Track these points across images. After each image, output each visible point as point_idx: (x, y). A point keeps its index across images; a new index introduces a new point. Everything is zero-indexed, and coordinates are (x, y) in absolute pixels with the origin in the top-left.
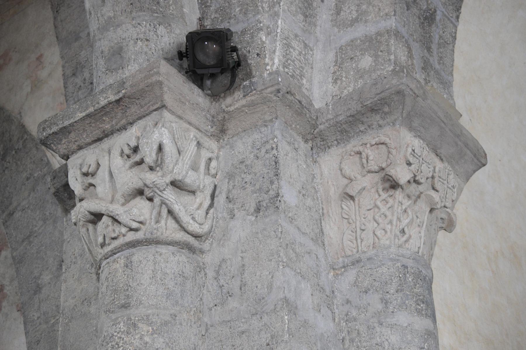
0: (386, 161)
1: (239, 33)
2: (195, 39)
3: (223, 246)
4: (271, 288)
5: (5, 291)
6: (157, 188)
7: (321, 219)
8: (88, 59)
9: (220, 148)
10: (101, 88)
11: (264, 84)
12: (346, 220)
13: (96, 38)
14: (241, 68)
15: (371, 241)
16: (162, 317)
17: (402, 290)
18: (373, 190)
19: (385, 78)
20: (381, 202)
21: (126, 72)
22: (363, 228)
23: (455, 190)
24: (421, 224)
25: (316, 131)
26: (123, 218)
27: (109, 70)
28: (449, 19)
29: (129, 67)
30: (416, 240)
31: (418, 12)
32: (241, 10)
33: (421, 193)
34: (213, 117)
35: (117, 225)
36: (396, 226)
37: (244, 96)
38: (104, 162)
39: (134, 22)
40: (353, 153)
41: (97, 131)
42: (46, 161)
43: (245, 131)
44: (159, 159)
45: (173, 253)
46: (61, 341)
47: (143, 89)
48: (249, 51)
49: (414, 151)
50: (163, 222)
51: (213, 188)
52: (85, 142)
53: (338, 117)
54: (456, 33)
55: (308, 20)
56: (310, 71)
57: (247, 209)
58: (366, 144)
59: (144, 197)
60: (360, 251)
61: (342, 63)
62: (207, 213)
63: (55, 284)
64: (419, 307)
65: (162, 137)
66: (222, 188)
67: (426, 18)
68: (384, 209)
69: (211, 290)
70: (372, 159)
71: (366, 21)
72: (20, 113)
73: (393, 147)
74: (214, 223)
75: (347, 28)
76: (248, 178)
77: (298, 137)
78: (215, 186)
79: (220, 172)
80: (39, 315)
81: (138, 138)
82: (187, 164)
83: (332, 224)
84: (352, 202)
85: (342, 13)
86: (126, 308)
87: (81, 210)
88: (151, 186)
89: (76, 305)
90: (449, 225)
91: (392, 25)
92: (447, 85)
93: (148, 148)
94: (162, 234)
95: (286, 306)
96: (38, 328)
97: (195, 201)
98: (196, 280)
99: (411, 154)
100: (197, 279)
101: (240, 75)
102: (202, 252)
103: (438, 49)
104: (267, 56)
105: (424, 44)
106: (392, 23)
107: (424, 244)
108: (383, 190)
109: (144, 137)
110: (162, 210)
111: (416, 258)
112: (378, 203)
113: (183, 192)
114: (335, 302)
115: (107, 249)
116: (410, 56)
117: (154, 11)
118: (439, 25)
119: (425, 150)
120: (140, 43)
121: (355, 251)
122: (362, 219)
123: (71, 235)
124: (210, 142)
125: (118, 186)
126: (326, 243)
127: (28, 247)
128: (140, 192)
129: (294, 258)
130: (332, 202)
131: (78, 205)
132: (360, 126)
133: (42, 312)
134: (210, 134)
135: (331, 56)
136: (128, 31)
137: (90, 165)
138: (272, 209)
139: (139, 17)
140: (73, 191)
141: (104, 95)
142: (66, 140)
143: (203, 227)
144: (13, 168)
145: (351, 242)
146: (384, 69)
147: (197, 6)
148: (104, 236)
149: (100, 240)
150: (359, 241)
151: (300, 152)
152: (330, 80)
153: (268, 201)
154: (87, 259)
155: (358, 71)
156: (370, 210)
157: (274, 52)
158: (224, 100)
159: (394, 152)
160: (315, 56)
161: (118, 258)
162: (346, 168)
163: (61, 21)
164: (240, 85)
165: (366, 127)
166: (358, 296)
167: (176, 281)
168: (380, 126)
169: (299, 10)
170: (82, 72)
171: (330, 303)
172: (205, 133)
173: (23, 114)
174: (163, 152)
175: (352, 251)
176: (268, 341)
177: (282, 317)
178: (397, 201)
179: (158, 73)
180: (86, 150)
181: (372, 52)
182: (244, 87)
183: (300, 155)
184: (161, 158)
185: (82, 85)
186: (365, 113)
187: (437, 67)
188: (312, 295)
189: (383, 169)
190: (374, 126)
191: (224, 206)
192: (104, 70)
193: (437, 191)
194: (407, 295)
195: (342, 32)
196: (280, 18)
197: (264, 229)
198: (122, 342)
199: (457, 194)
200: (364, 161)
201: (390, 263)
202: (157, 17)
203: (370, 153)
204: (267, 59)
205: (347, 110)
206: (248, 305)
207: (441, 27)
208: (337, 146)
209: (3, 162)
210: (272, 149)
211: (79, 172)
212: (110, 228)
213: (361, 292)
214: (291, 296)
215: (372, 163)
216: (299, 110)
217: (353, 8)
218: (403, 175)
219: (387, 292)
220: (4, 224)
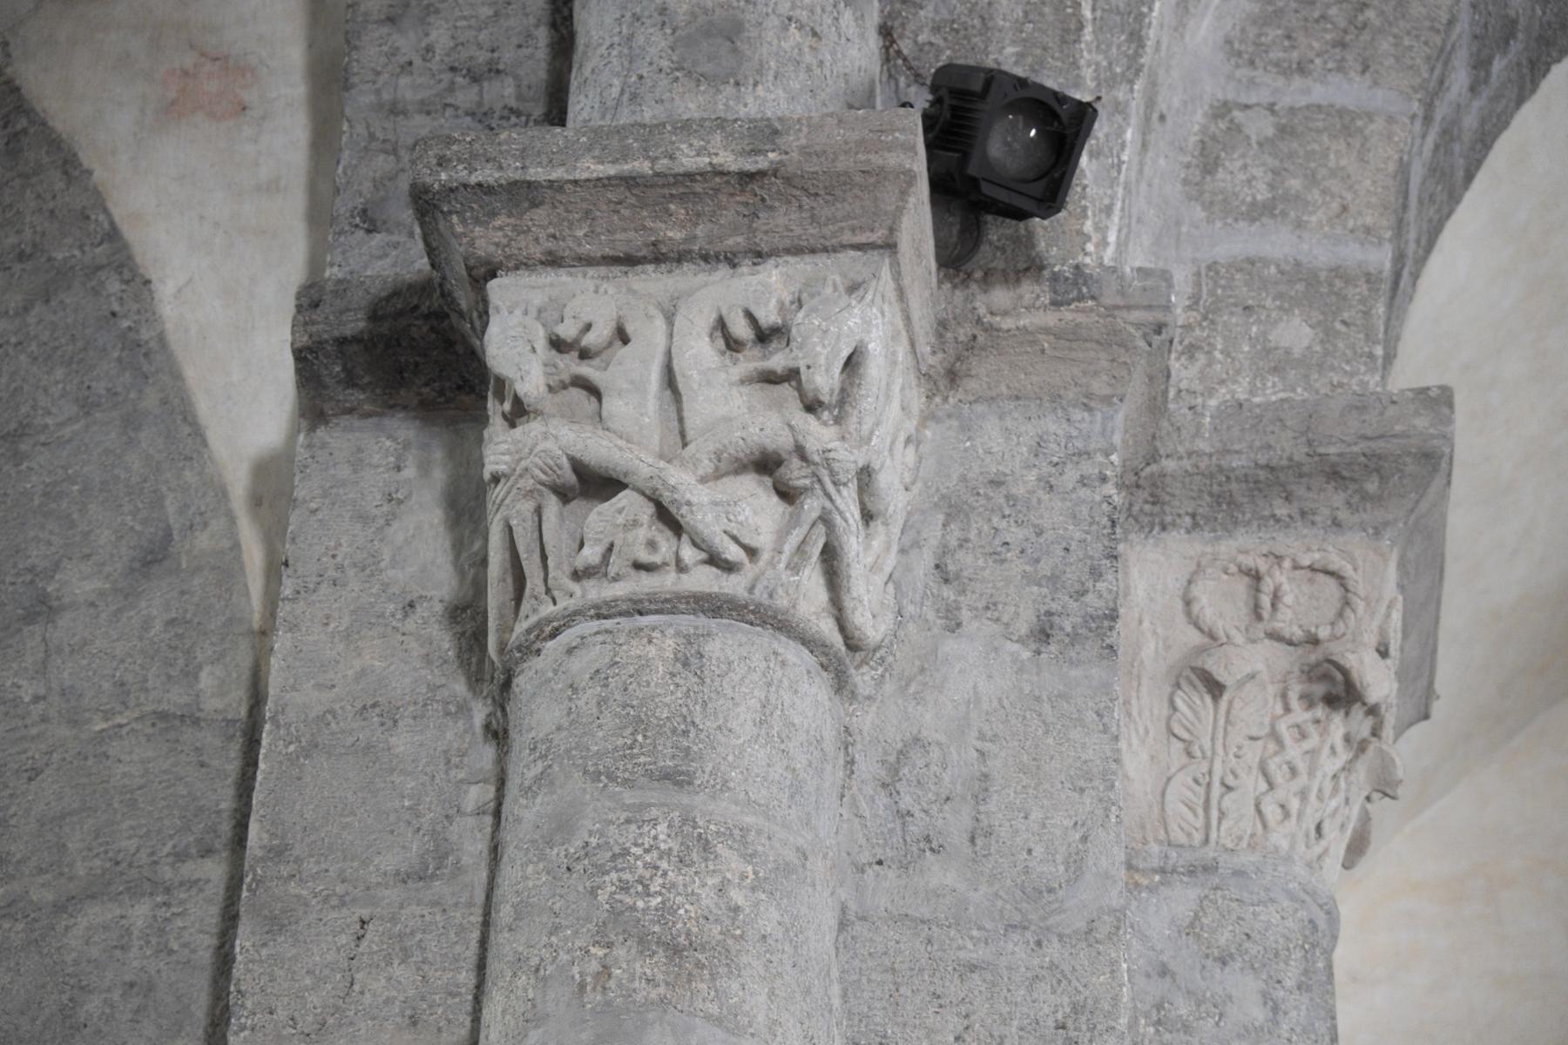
3: (918, 698)
12: (1180, 745)
17: (1309, 989)
19: (1394, 402)
22: (1230, 780)
25: (1148, 470)
29: (760, 90)
38: (650, 335)
40: (1233, 568)
41: (631, 234)
42: (106, 225)
43: (1017, 398)
47: (846, 173)
52: (580, 250)
53: (1228, 457)
57: (1005, 619)
68: (1294, 752)
73: (1362, 593)
75: (1236, 220)
76: (1016, 535)
80: (42, 692)
83: (1135, 741)
84: (1208, 699)
85: (1221, 174)
86: (680, 784)
88: (817, 458)
104: (1090, 213)
112: (1283, 727)
115: (596, 591)
120: (797, 34)
121: (1198, 837)
122: (1231, 756)
128: (766, 464)
130: (1145, 681)
132: (1278, 502)
142: (512, 221)
145: (1190, 808)
150: (1214, 814)
159: (1361, 606)
168: (1336, 523)
175: (1189, 835)
176: (1060, 1016)
185: (417, 61)
186: (1309, 475)
190: (1318, 519)
195: (1219, 224)
198: (660, 881)
200: (1266, 600)
201: (1286, 903)
203: (1286, 587)
205: (1261, 448)
206: (997, 895)
212: (642, 533)
215: (1285, 614)
219: (1279, 982)
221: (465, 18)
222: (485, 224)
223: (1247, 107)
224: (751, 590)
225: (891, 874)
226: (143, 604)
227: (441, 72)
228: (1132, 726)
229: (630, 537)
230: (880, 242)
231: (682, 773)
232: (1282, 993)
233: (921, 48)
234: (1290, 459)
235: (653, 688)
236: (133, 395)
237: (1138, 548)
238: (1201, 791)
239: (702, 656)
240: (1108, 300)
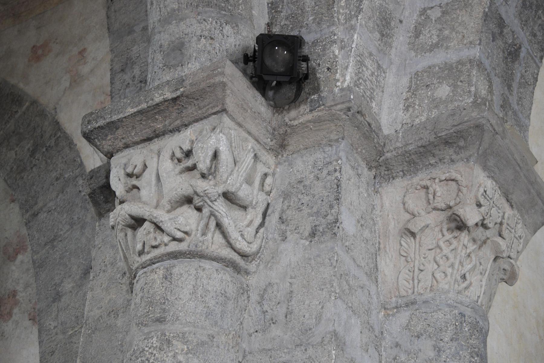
0: (455, 199)
1: (310, 43)
2: (267, 41)
4: (320, 319)
5: (17, 297)
6: (208, 197)
7: (376, 254)
8: (140, 55)
9: (278, 164)
10: (156, 84)
11: (334, 100)
12: (404, 258)
13: (156, 31)
14: (308, 81)
15: (429, 284)
16: (198, 336)
17: (457, 340)
18: (437, 229)
19: (464, 109)
20: (444, 242)
21: (186, 70)
22: (422, 267)
23: (522, 241)
24: (483, 272)
25: (381, 159)
26: (167, 226)
27: (167, 66)
28: (533, 58)
29: (190, 65)
30: (477, 289)
31: (503, 45)
32: (314, 19)
33: (488, 238)
34: (274, 129)
35: (159, 233)
36: (458, 270)
37: (311, 111)
38: (152, 165)
39: (199, 17)
40: (419, 187)
41: (147, 130)
42: (80, 162)
43: (307, 148)
44: (213, 167)
45: (217, 270)
46: (81, 353)
48: (319, 64)
49: (485, 191)
50: (210, 235)
51: (266, 205)
52: (133, 140)
53: (408, 147)
54: (538, 74)
55: (385, 39)
56: (380, 94)
57: (301, 232)
58: (435, 179)
59: (192, 206)
60: (416, 293)
61: (416, 90)
62: (257, 232)
63: (77, 294)
64: (473, 360)
65: (219, 143)
66: (276, 208)
67: (510, 54)
68: (446, 250)
69: (253, 315)
70: (440, 195)
71: (447, 48)
72: (56, 108)
73: (464, 185)
74: (263, 244)
75: (425, 53)
76: (306, 199)
77: (363, 163)
78: (268, 204)
79: (275, 189)
80: (56, 324)
81: (192, 142)
82: (242, 176)
83: (388, 261)
84: (412, 239)
85: (421, 37)
86: (161, 322)
87: (120, 213)
88: (202, 194)
89: (101, 316)
90: (510, 277)
91: (476, 54)
92: (523, 128)
93: (202, 154)
94: (207, 248)
95: (335, 340)
96: (53, 338)
97: (246, 218)
98: (238, 302)
99: (483, 195)
100: (240, 301)
101: (307, 89)
102: (247, 273)
103: (518, 88)
104: (338, 71)
105: (505, 80)
106: (476, 52)
107: (484, 293)
108: (448, 230)
109: (199, 141)
110: (210, 223)
111: (475, 307)
112: (441, 243)
113: (234, 206)
114: (383, 344)
115: (146, 258)
116: (491, 91)
117: (223, 9)
118: (522, 62)
119: (496, 193)
120: (204, 40)
121: (410, 291)
122: (422, 258)
123: (103, 241)
124: (268, 156)
125: (165, 191)
126: (379, 280)
127: (51, 252)
128: (188, 200)
129: (347, 290)
130: (391, 237)
131: (118, 207)
132: (430, 158)
133: (60, 322)
134: (268, 148)
135: (405, 81)
136: (191, 26)
137: (136, 166)
138: (328, 235)
139: (206, 12)
140: (114, 192)
141: (160, 92)
142: (112, 136)
143: (251, 246)
144: (42, 167)
145: (407, 282)
146: (462, 101)
147: (266, 10)
148: (144, 243)
149: (139, 247)
150: (416, 281)
151: (362, 179)
152: (401, 106)
153: (325, 226)
154: (118, 268)
155: (434, 100)
156: (432, 249)
157: (347, 68)
158: (288, 113)
159: (464, 190)
160: (387, 79)
161: (157, 268)
162: (410, 202)
163: (115, 11)
164: (307, 99)
165: (437, 160)
166: (409, 341)
167: (217, 300)
169: (376, 27)
170: (132, 68)
171: (378, 344)
172: (263, 146)
173: (58, 110)
174: (218, 159)
175: (407, 292)
177: (330, 352)
178: (461, 244)
179: (223, 74)
180: (133, 149)
181: (451, 81)
182: (312, 101)
183: (362, 182)
184: (215, 166)
185: (131, 82)
186: (438, 145)
187: (516, 107)
188: (361, 332)
189: (450, 208)
190: (445, 160)
191: (276, 226)
192: (161, 65)
193: (504, 239)
194: (462, 345)
195: (419, 56)
196: (357, 32)
197: (318, 256)
198: (153, 358)
199: (523, 246)
200: (431, 196)
202: (225, 15)
203: (438, 189)
204: (338, 75)
205: (419, 140)
206: (293, 335)
207: (524, 65)
208: (402, 178)
209: (32, 159)
210: (335, 171)
211: (122, 172)
212: (152, 235)
213: (412, 336)
214: (340, 330)
216: (367, 133)
217: (434, 32)
218: (472, 216)
220: (26, 224)
221: (143, 63)
222: (105, 140)
223: (432, 8)
224: (189, 247)
225: (260, 335)
226: (84, 288)
227: (137, 84)
228: (387, 256)
229: (148, 237)
230: (220, 110)
231: (162, 318)
232: (442, 344)
233: (282, 27)
234: (429, 141)
235: (156, 290)
236: (84, 218)
237: (385, 188)
238: (411, 274)
239: (172, 274)
240: (328, 104)
